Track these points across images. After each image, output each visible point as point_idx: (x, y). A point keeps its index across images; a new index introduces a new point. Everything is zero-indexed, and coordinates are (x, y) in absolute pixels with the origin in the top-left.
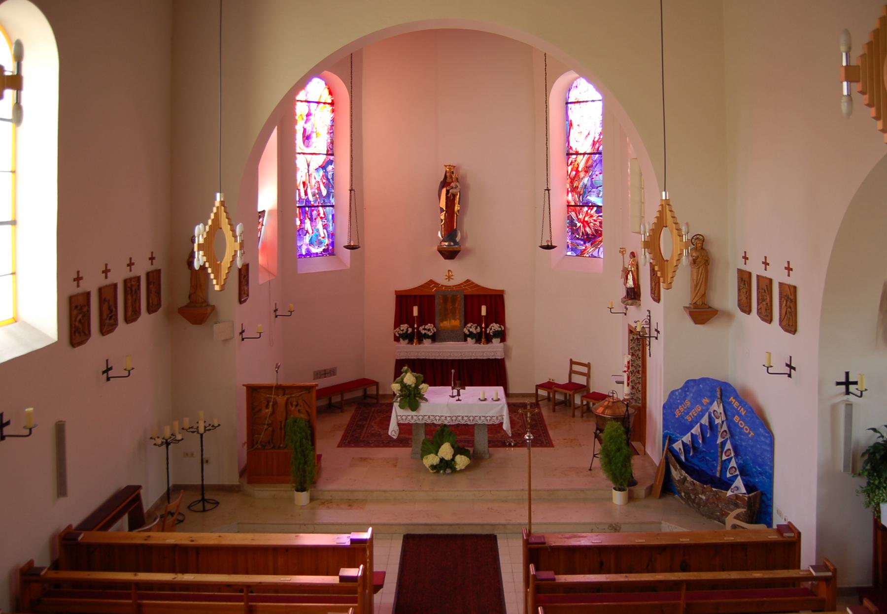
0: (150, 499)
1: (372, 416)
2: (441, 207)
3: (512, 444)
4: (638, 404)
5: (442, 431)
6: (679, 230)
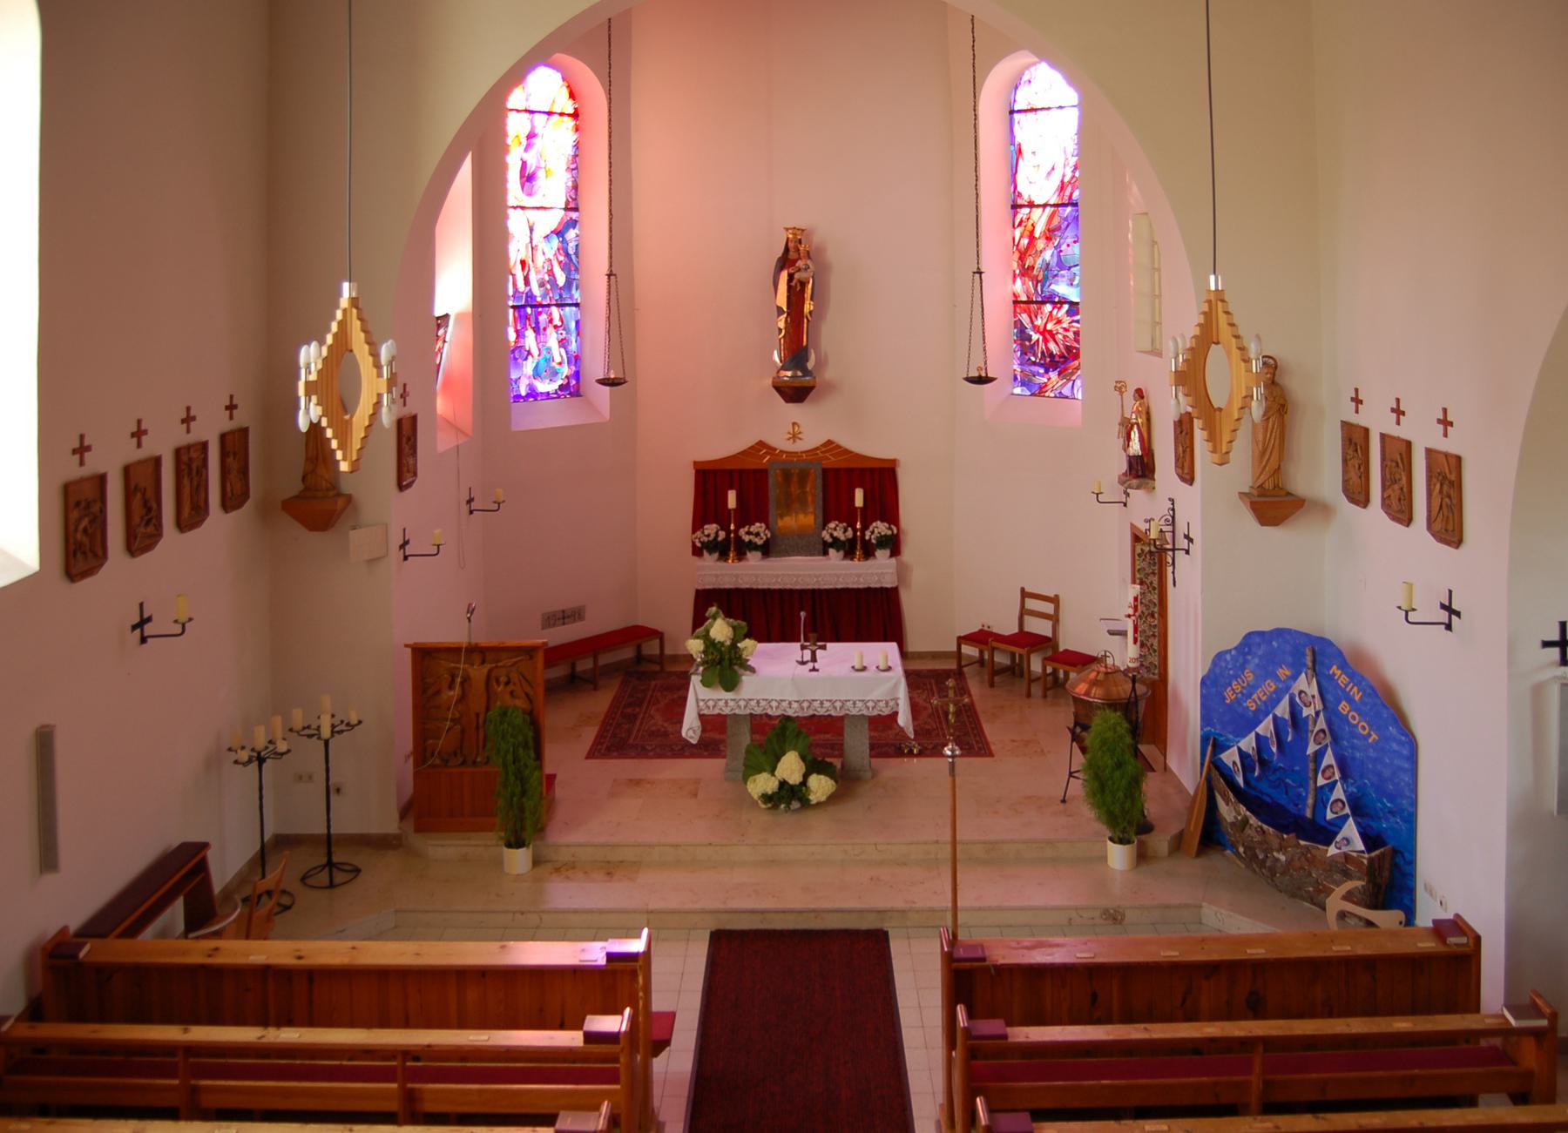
0: (225, 867)
1: (651, 697)
2: (779, 305)
3: (915, 751)
4: (1151, 676)
5: (784, 729)
6: (1242, 349)
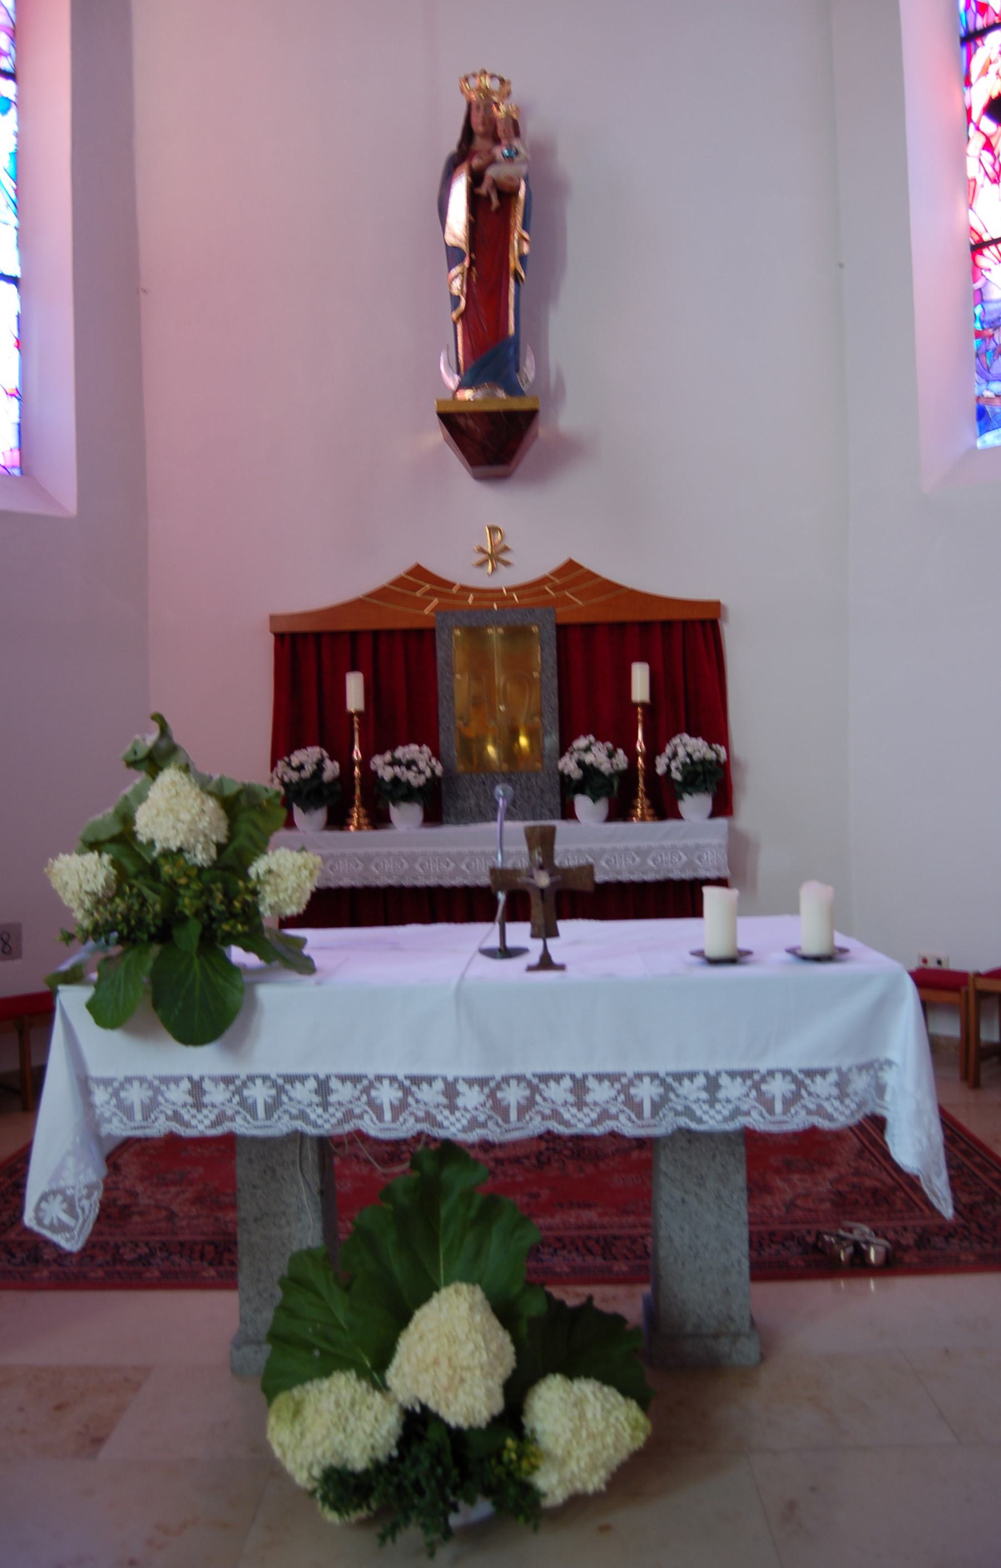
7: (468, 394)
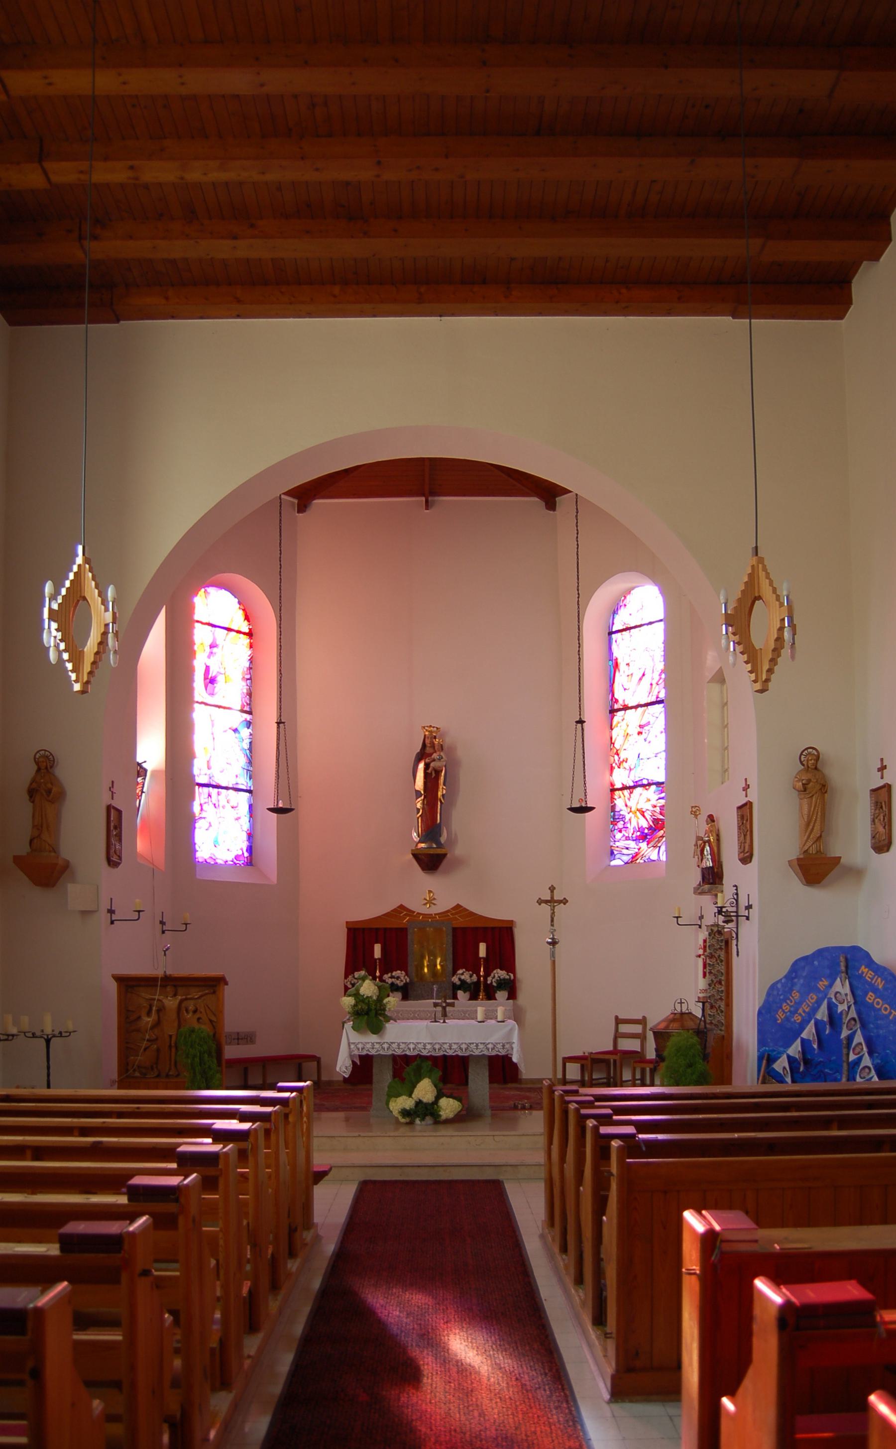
4: (719, 1032)
7: (423, 845)
